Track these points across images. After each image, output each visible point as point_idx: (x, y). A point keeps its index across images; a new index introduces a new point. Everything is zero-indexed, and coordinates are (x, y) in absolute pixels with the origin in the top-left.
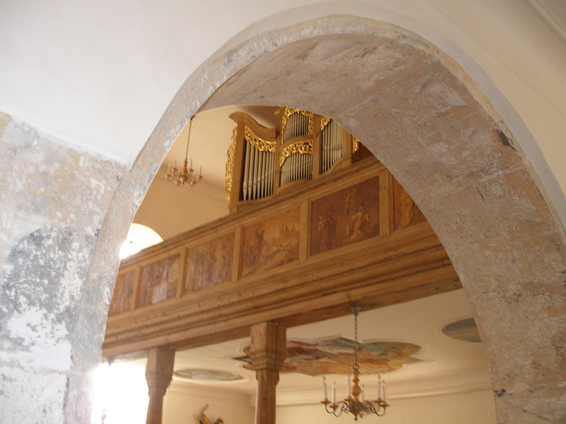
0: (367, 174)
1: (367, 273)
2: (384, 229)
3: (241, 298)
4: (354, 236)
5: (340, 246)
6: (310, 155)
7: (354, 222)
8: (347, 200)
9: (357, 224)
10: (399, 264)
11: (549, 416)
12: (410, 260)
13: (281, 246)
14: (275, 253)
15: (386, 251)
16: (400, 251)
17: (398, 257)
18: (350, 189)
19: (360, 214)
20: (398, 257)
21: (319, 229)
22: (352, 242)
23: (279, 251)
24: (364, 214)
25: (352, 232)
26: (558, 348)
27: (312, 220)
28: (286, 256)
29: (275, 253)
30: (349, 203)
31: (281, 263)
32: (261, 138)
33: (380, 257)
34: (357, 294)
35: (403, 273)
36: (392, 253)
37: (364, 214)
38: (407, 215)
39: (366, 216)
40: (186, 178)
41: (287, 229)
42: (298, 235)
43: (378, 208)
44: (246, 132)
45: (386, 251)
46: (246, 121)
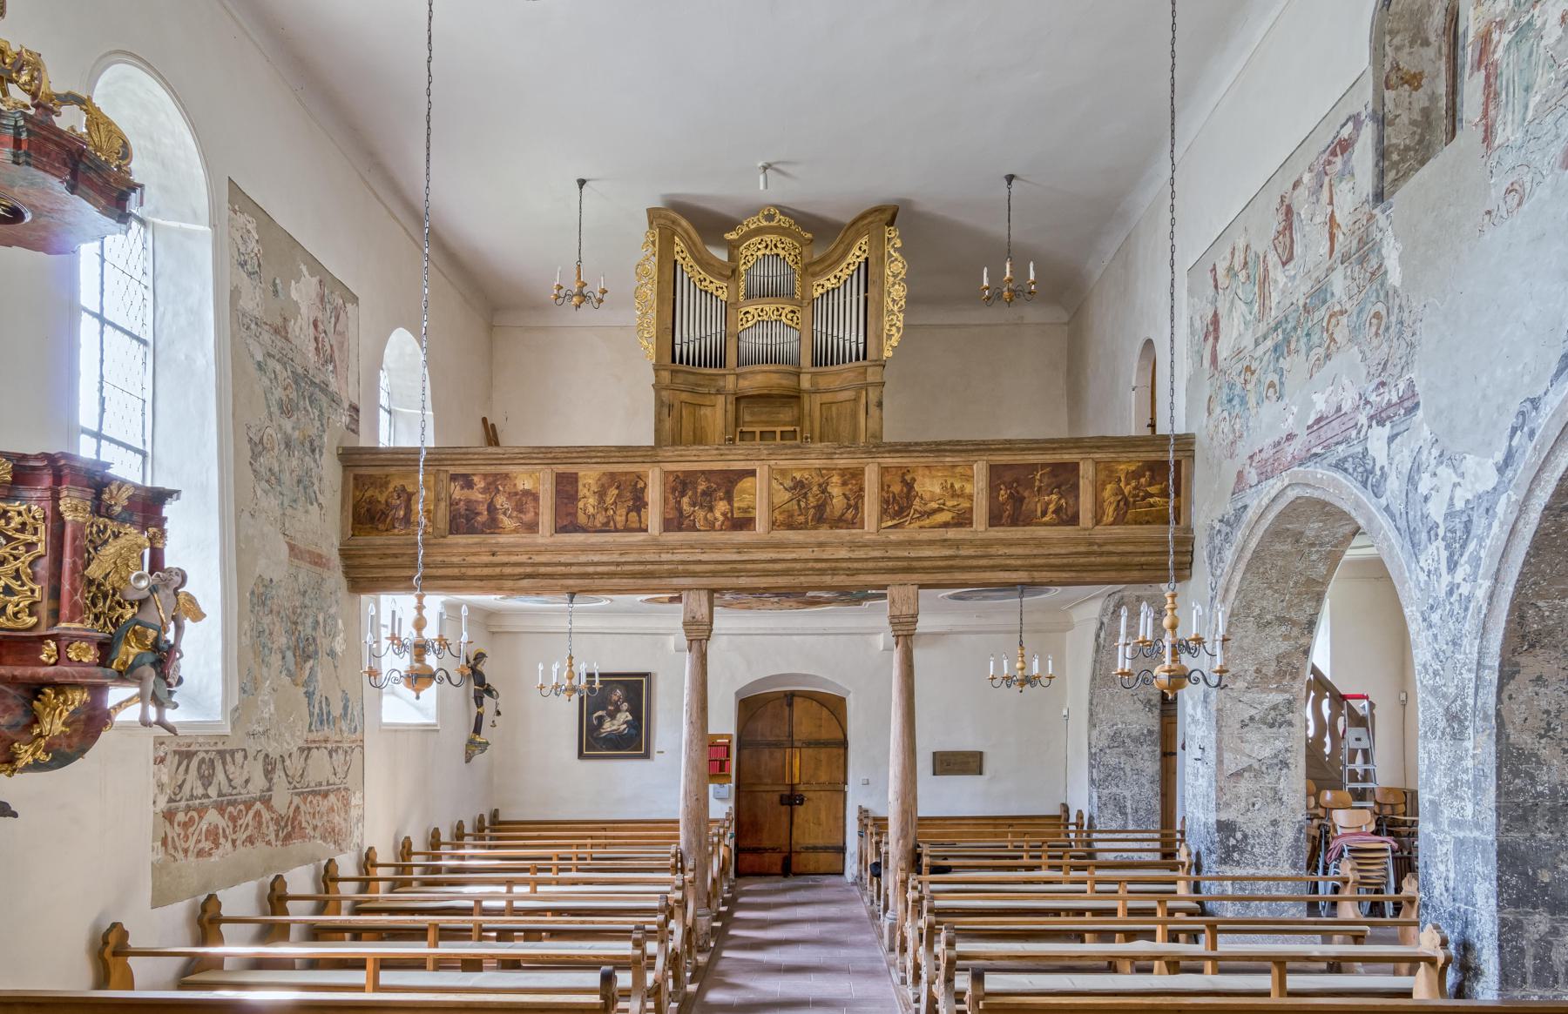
0: (1066, 456)
1: (1065, 561)
2: (1086, 517)
3: (887, 555)
4: (1046, 519)
5: (1029, 524)
6: (706, 292)
7: (1048, 503)
8: (1038, 477)
9: (1052, 507)
10: (1098, 560)
11: (1258, 706)
12: (1115, 559)
13: (944, 504)
14: (934, 511)
15: (1091, 544)
16: (1105, 549)
17: (1101, 554)
18: (1044, 466)
19: (1054, 497)
20: (1101, 554)
21: (1000, 498)
22: (1046, 524)
23: (940, 510)
24: (1060, 499)
25: (1044, 513)
26: (1278, 662)
27: (993, 488)
28: (953, 518)
29: (934, 511)
30: (1041, 481)
31: (946, 525)
32: (701, 268)
33: (1082, 549)
34: (1039, 576)
35: (1100, 568)
36: (1095, 548)
37: (1060, 499)
38: (1111, 514)
39: (1063, 501)
40: (583, 297)
41: (952, 486)
42: (970, 497)
43: (1077, 497)
44: (677, 249)
45: (1091, 544)
46: (679, 230)
